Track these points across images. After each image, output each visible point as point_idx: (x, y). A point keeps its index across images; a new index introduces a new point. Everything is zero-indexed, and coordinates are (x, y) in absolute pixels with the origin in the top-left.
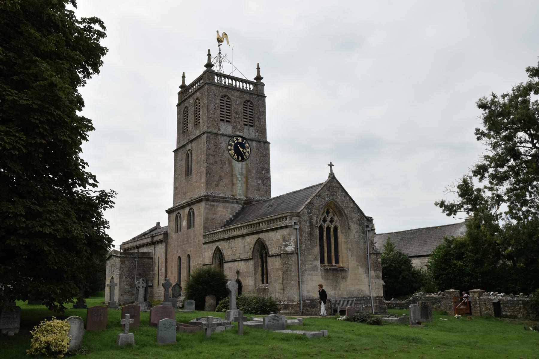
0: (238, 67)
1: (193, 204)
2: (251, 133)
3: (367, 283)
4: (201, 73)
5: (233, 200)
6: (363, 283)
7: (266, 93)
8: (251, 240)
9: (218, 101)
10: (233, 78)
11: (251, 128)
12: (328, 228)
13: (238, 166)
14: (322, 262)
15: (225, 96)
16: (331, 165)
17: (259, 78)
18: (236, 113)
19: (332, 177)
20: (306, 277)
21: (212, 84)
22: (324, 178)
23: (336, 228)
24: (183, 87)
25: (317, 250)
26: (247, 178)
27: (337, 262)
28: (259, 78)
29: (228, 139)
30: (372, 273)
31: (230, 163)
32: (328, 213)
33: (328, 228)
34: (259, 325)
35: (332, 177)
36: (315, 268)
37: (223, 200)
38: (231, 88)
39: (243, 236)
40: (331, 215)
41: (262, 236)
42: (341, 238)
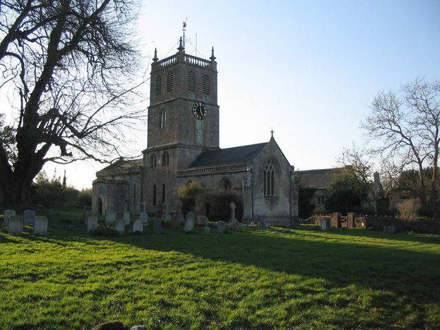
0: (198, 50)
1: (168, 149)
2: (206, 99)
3: (289, 207)
4: (175, 53)
5: (196, 147)
6: (285, 206)
7: (218, 69)
8: (218, 178)
9: (187, 75)
10: (196, 58)
11: (208, 96)
12: (269, 172)
13: (199, 123)
14: (265, 194)
15: (191, 72)
16: (272, 132)
17: (213, 58)
18: (198, 84)
19: (272, 139)
20: (256, 203)
21: (183, 62)
22: (268, 140)
23: (273, 172)
24: (155, 59)
25: (262, 186)
26: (204, 131)
27: (272, 194)
28: (213, 58)
29: (193, 103)
30: (293, 201)
31: (194, 121)
32: (269, 162)
33: (269, 172)
34: (416, 232)
35: (272, 139)
36: (260, 197)
37: (189, 147)
38: (197, 66)
39: (212, 175)
40: (270, 164)
41: (228, 175)
42: (276, 179)
